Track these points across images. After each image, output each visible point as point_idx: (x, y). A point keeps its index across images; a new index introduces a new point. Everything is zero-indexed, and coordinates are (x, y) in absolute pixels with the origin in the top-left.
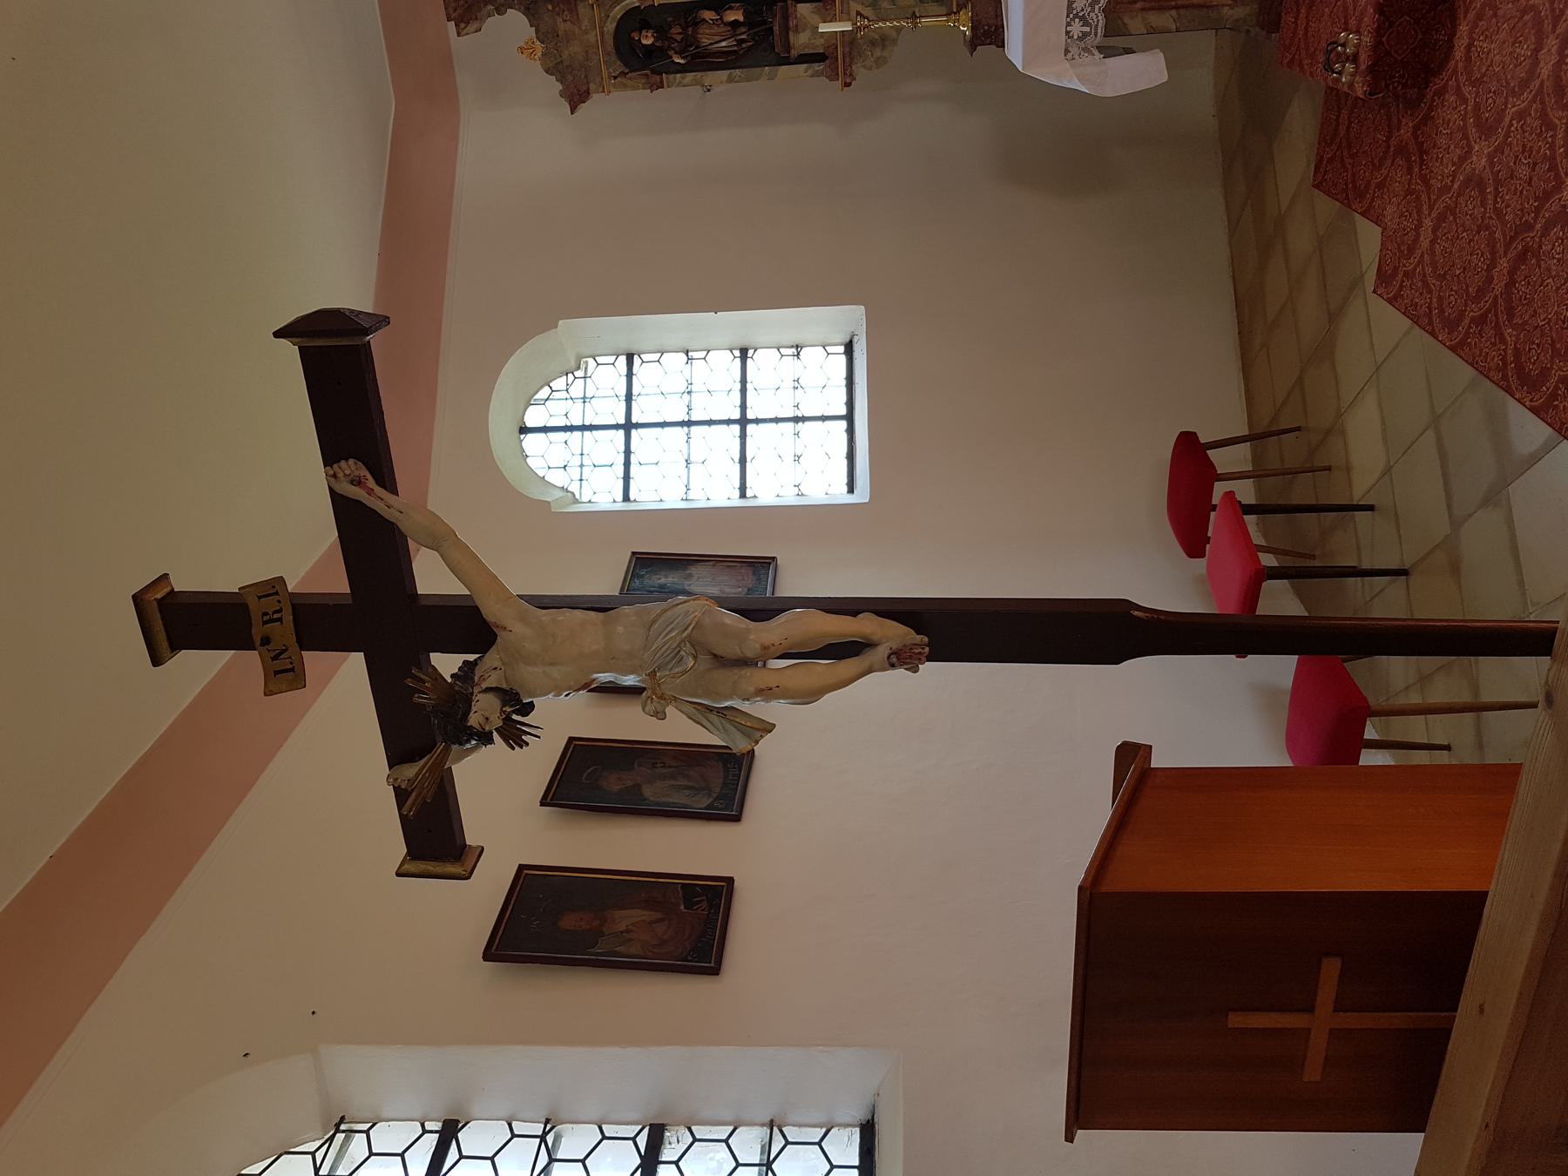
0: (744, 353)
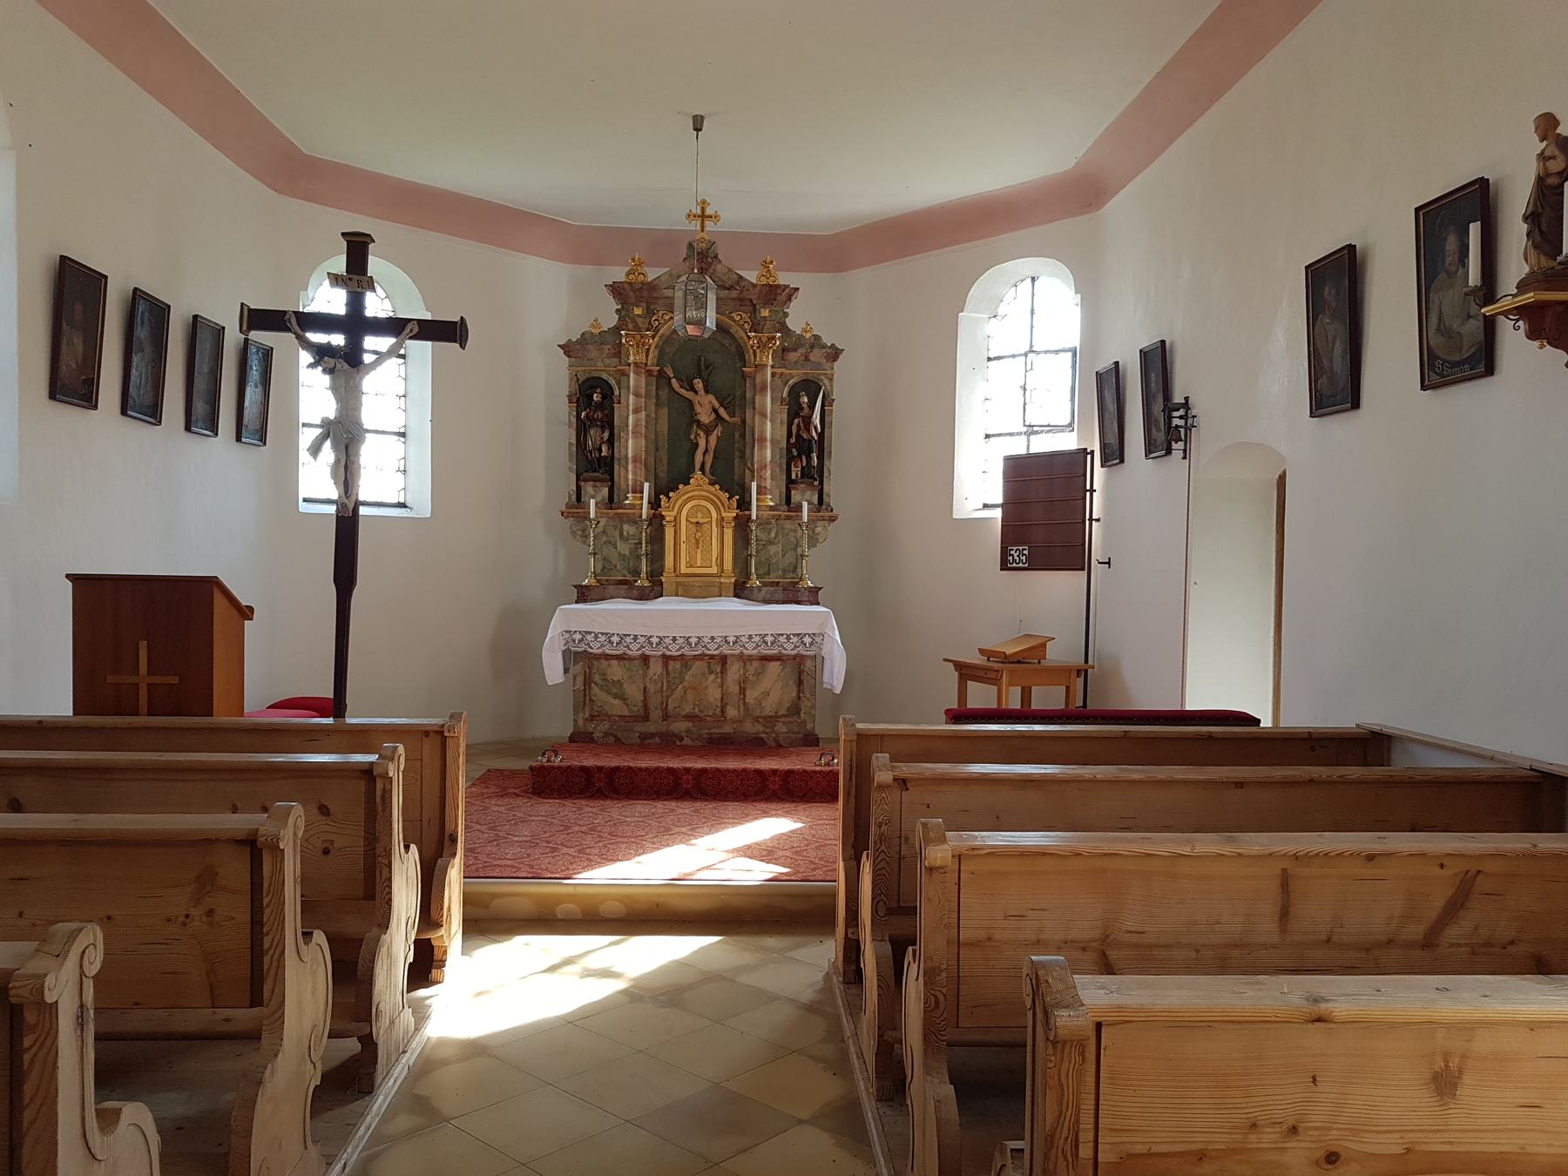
0: (403, 435)
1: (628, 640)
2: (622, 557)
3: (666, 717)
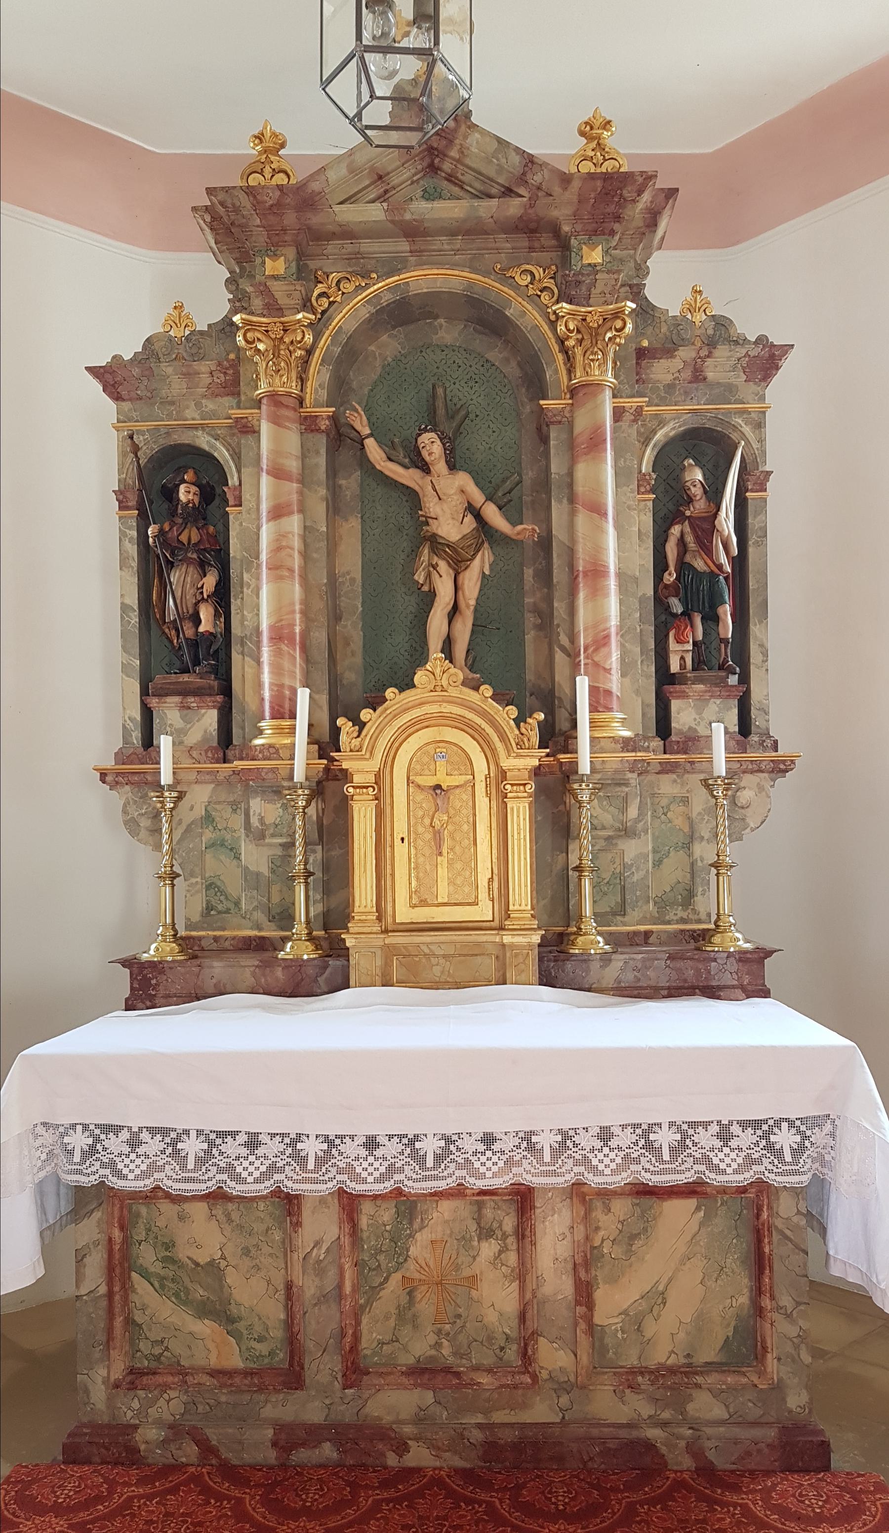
1: (232, 1148)
2: (253, 880)
3: (355, 1371)
